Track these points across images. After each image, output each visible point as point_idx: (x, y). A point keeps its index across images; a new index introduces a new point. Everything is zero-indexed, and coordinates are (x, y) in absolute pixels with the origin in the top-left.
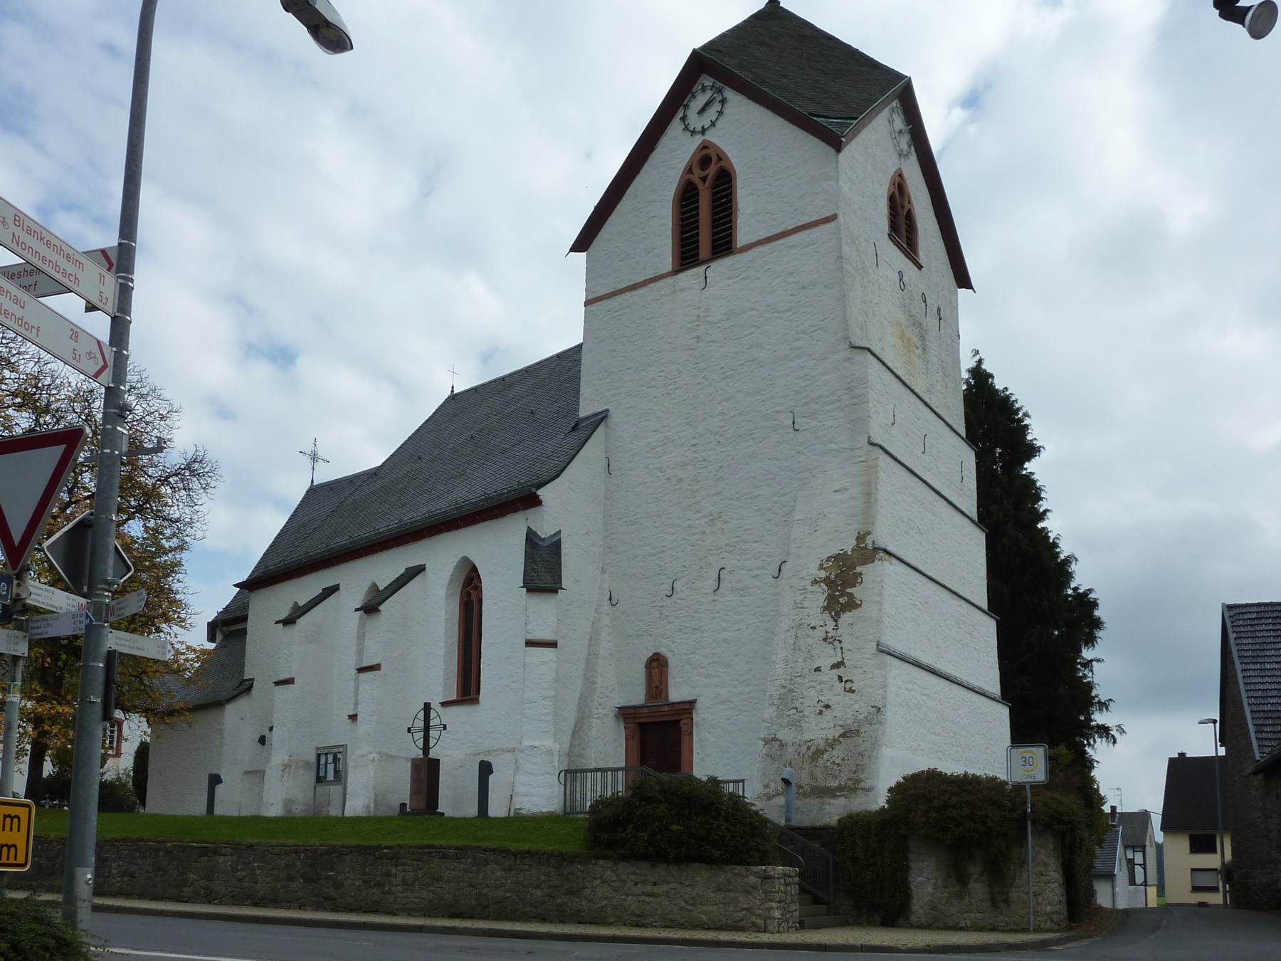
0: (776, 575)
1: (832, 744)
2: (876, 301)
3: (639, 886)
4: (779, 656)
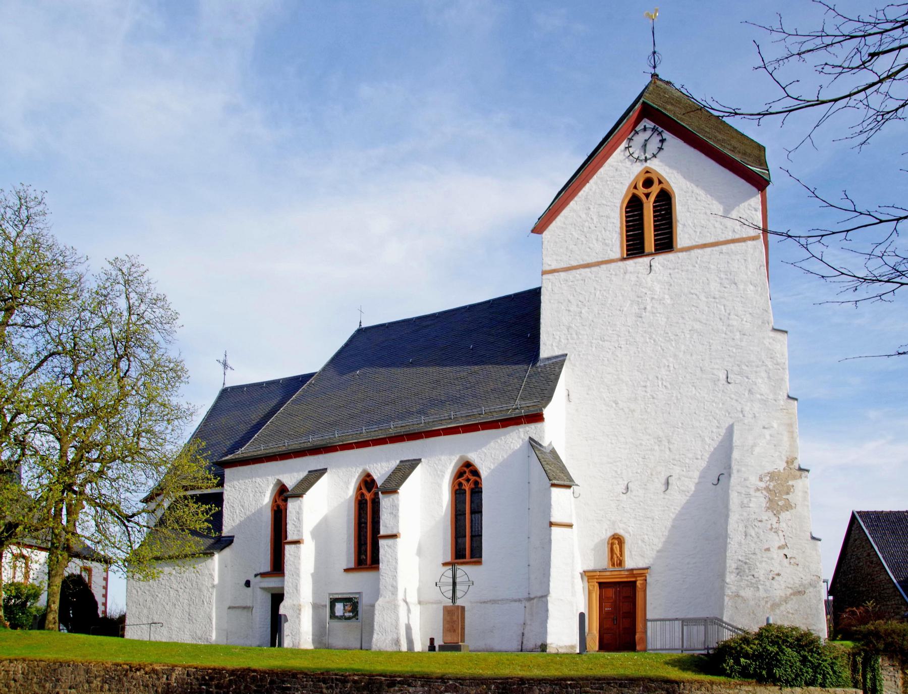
1: (786, 600)
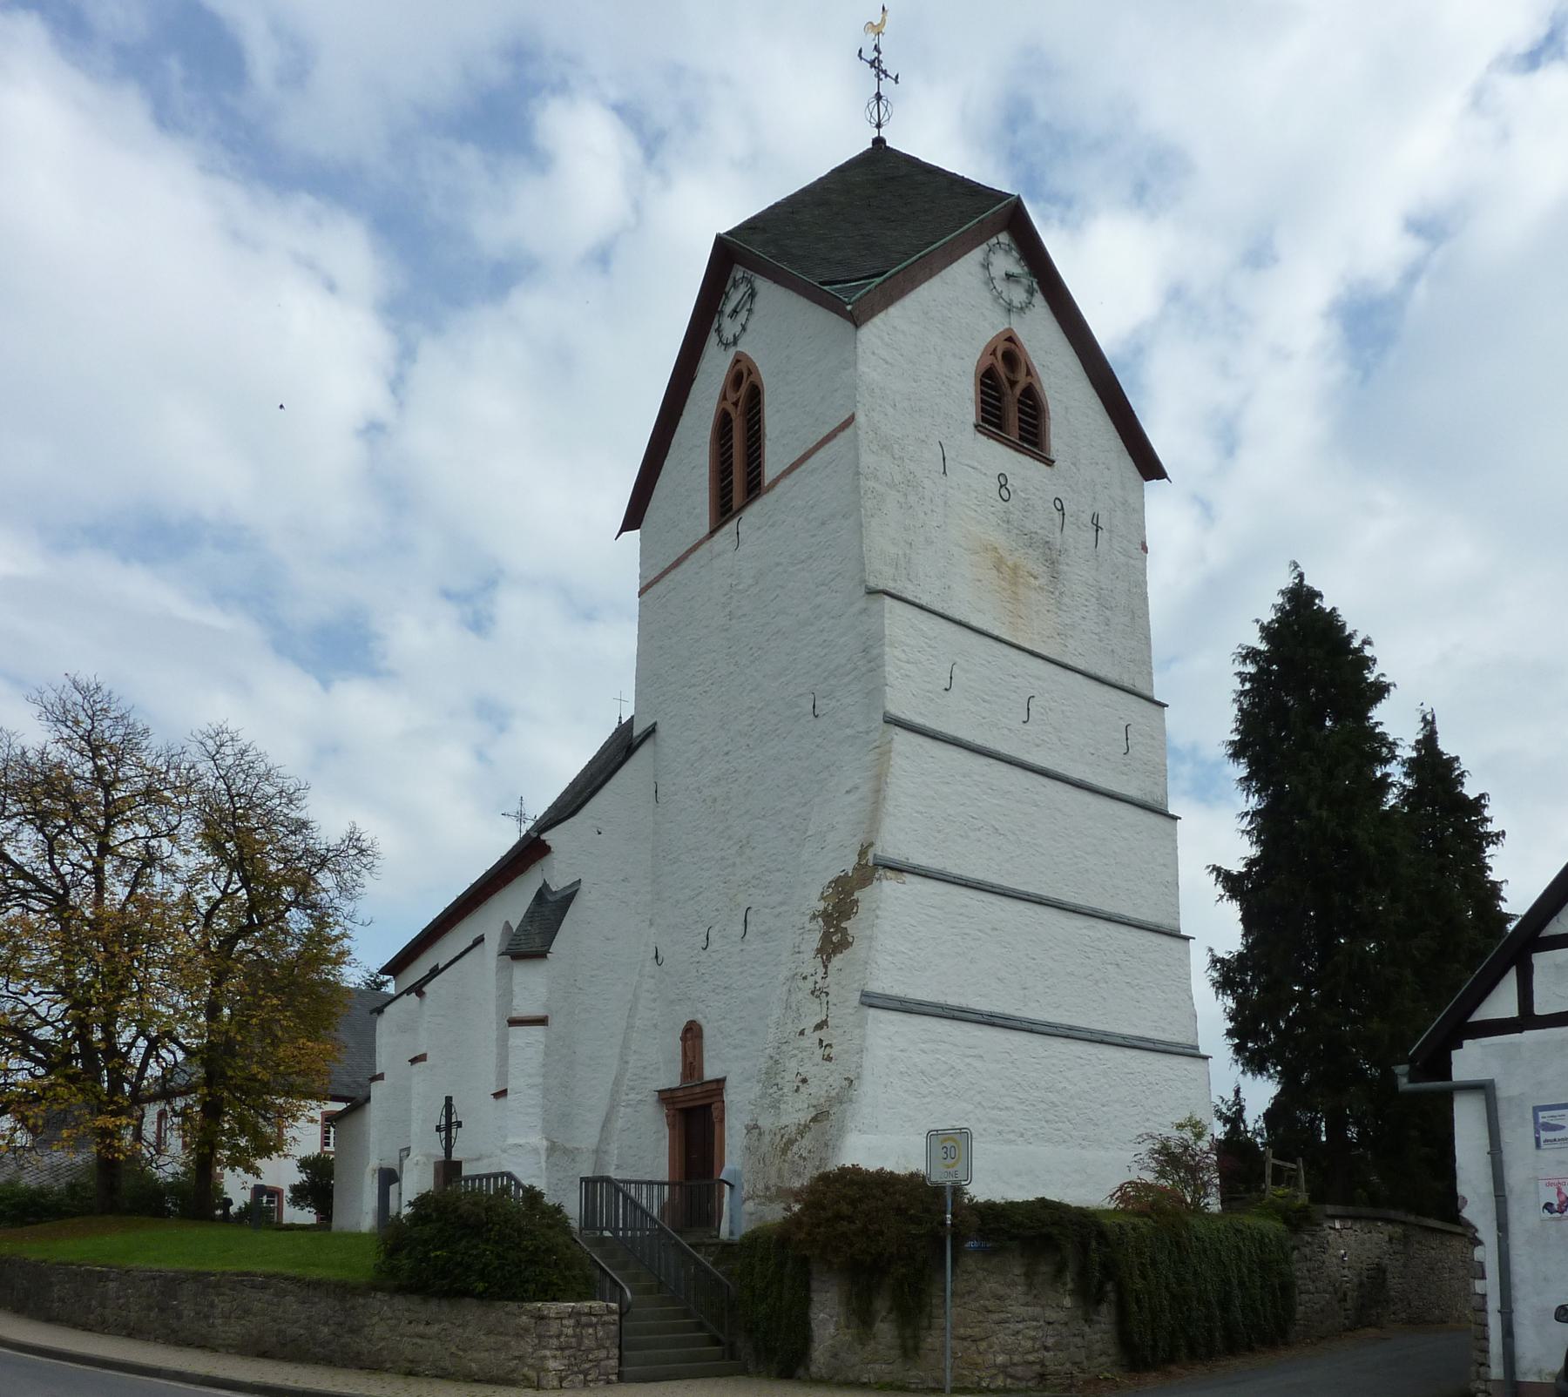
1: (803, 1130)
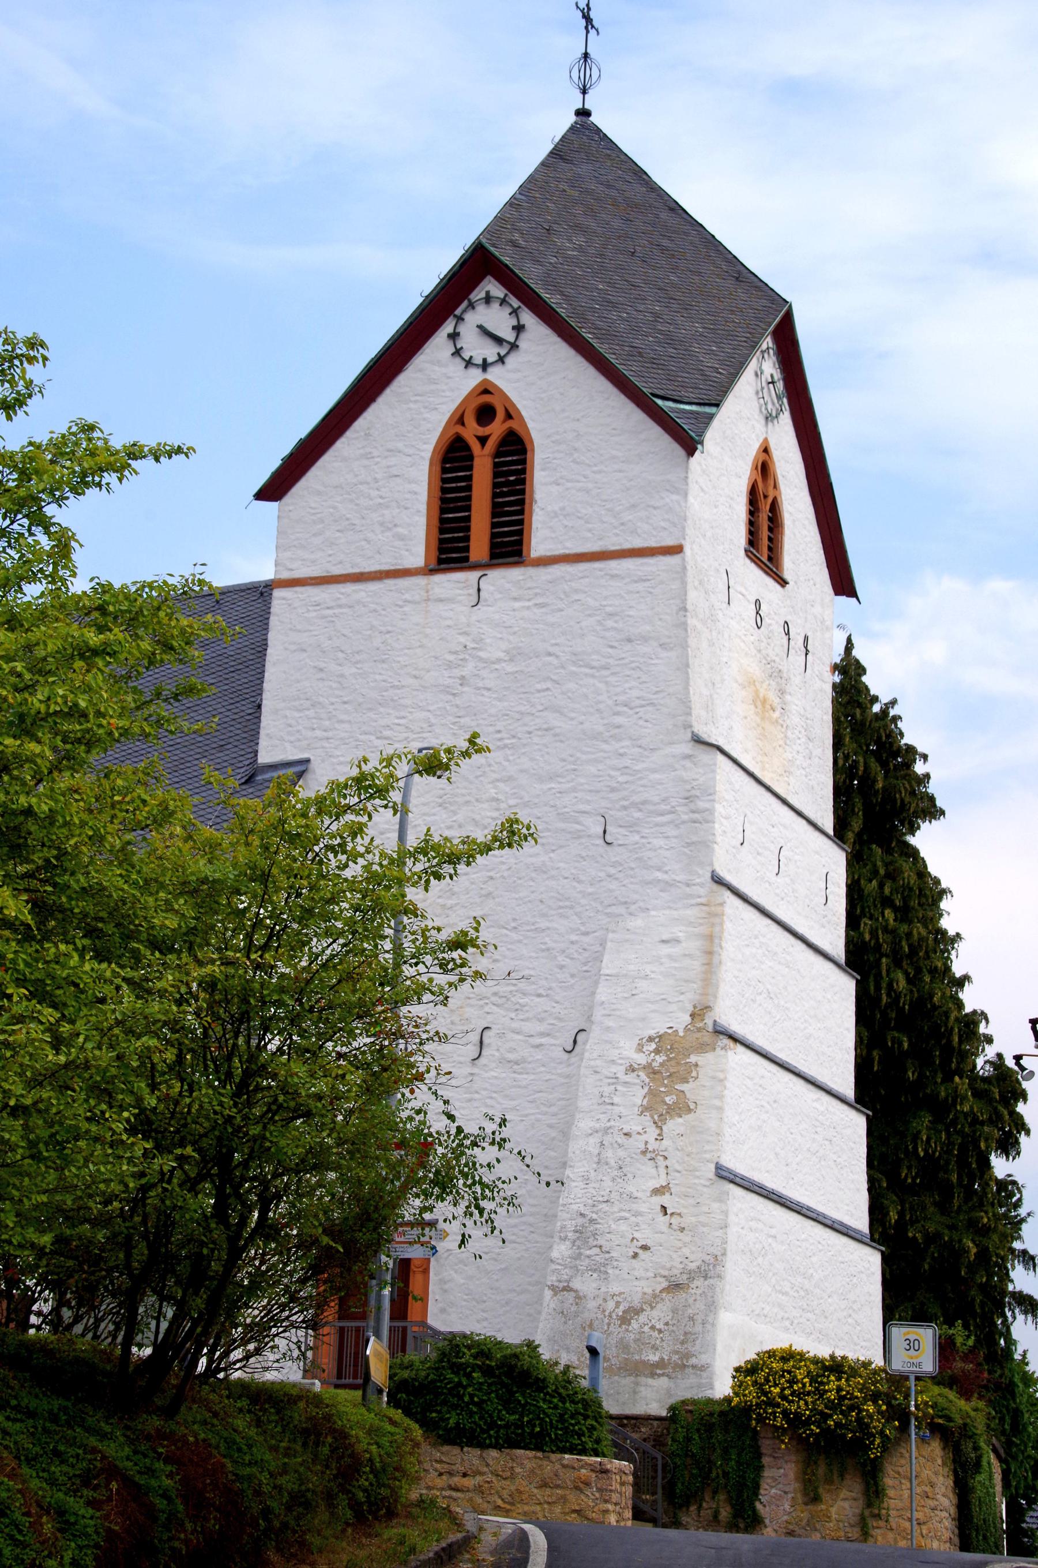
0: (569, 1048)
1: (652, 1301)
2: (725, 660)
3: (444, 1477)
4: (576, 1170)
